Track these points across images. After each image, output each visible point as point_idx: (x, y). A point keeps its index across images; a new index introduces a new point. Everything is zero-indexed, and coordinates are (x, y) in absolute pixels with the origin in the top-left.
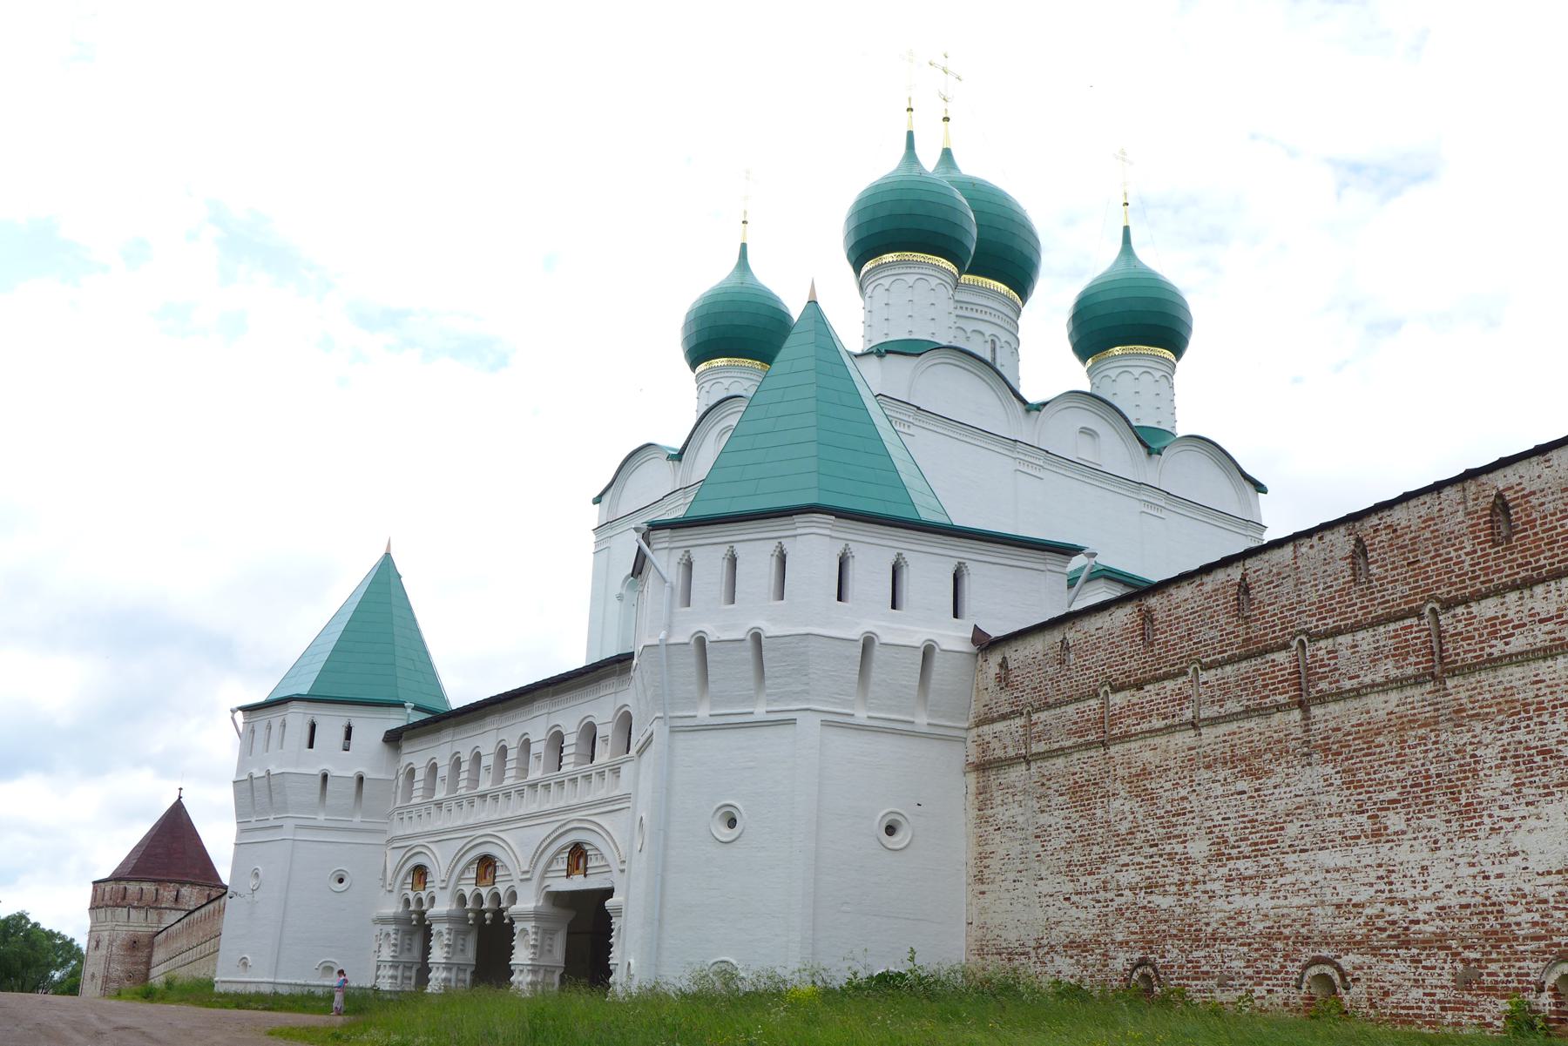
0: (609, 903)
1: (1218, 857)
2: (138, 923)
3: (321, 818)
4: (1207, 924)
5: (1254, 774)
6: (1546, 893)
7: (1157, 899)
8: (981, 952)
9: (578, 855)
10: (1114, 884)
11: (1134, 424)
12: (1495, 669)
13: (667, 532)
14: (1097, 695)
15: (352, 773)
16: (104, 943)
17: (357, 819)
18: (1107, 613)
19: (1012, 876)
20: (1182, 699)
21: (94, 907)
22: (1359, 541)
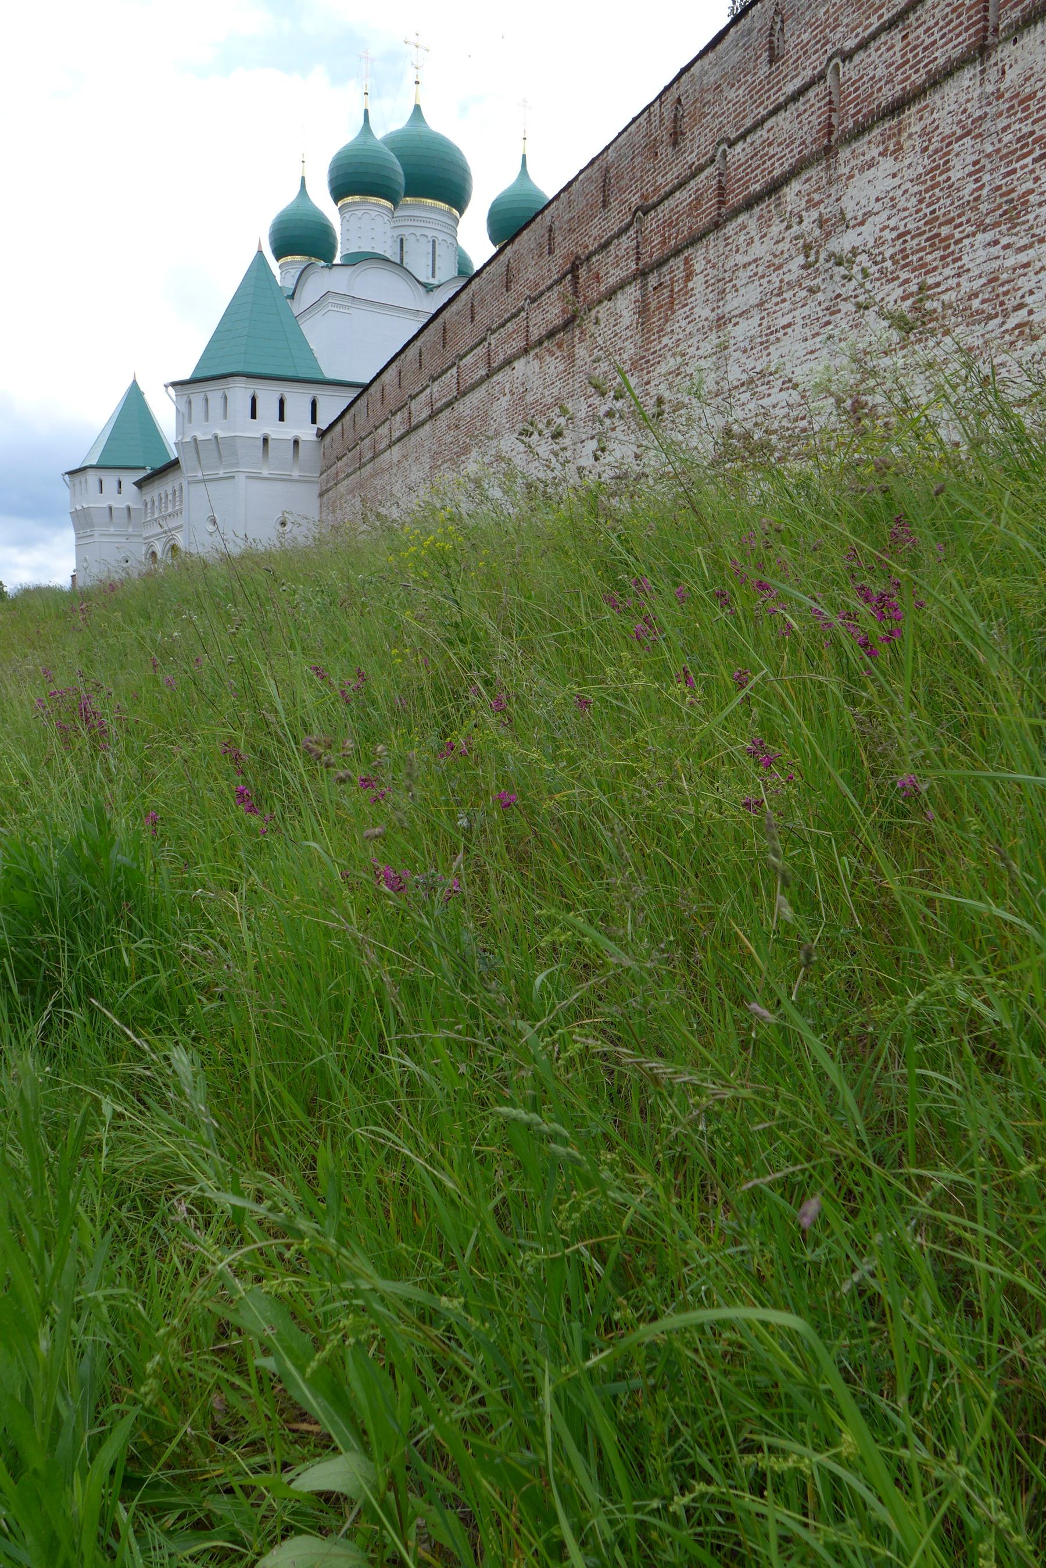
3: (112, 529)
17: (130, 529)
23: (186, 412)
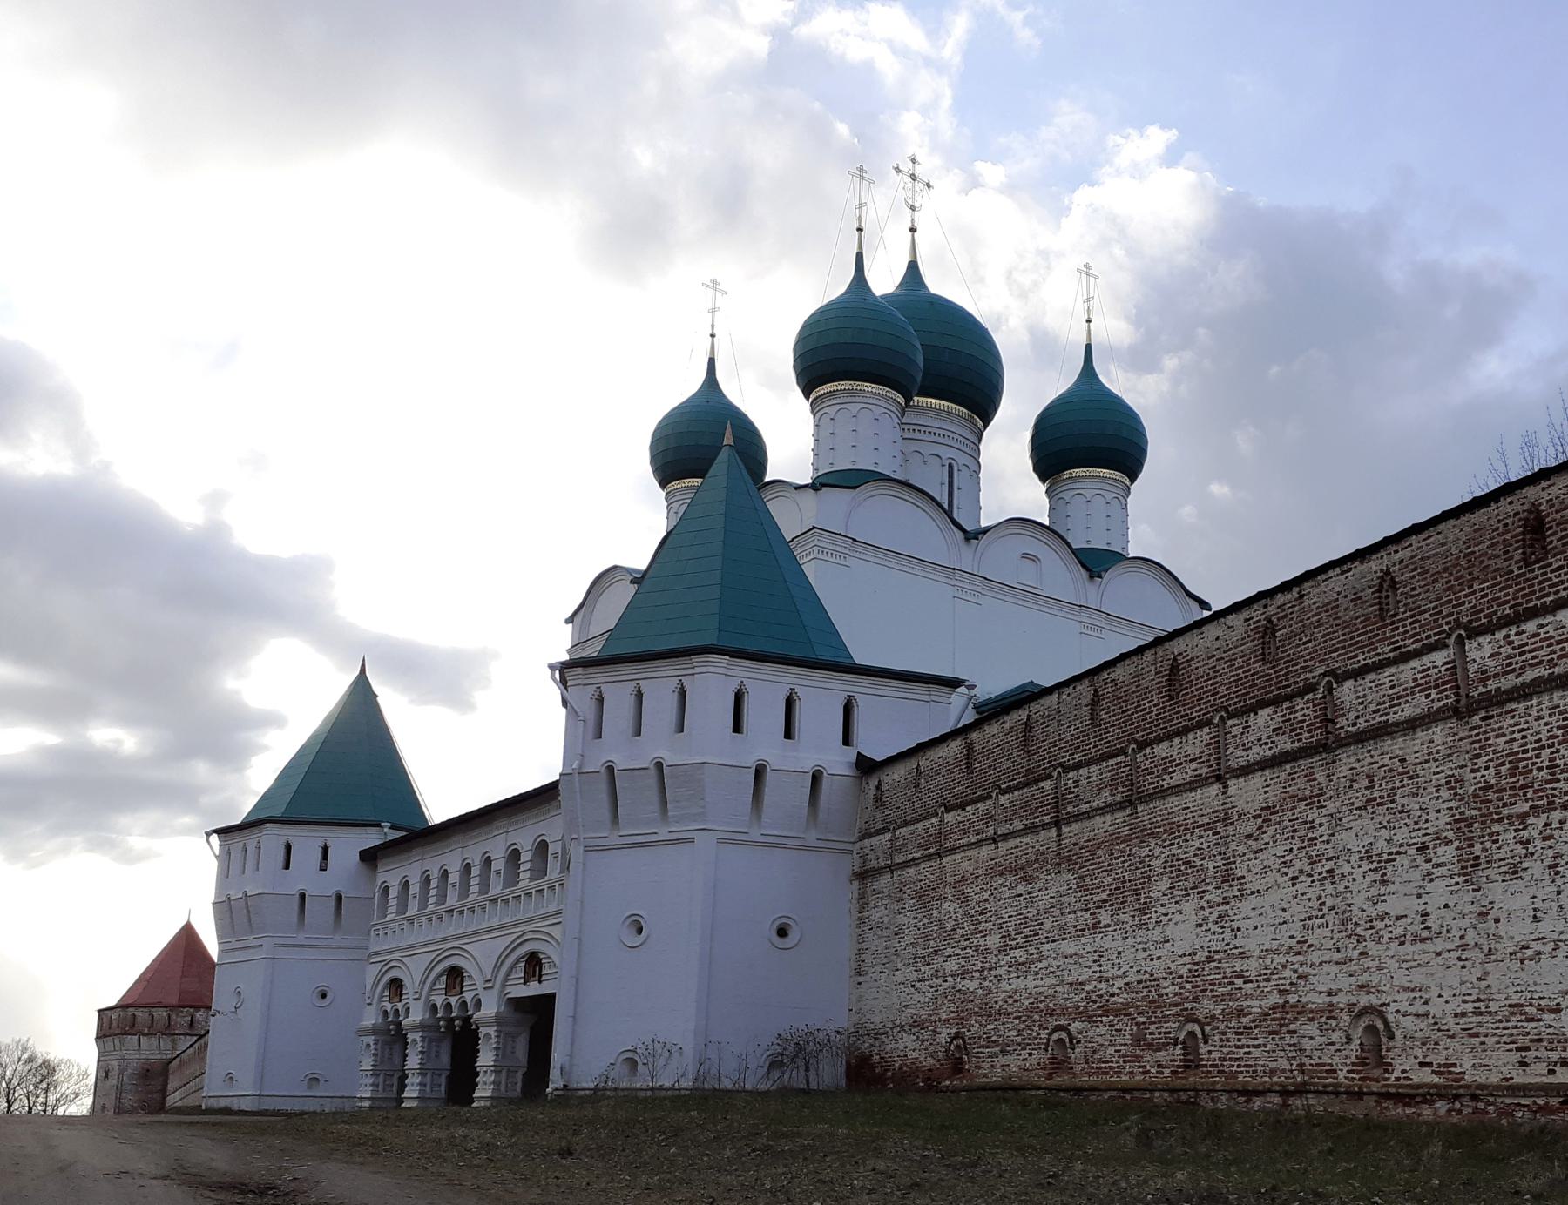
1: (1004, 948)
2: (150, 1050)
5: (1028, 880)
6: (1183, 970)
9: (534, 965)
12: (1164, 798)
13: (580, 670)
17: (337, 937)
20: (988, 818)
21: (100, 1036)
22: (1096, 691)
23: (591, 716)
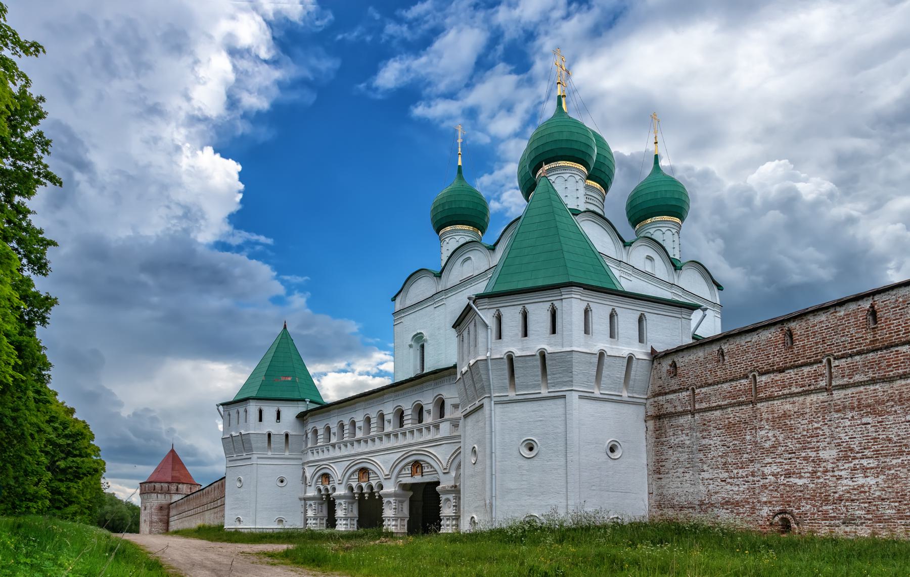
0: (438, 488)
3: (270, 454)
4: (835, 493)
5: (875, 413)
7: (794, 480)
8: (659, 506)
10: (760, 473)
11: (671, 256)
13: (486, 300)
14: (747, 377)
15: (283, 432)
16: (148, 508)
18: (755, 333)
19: (681, 470)
